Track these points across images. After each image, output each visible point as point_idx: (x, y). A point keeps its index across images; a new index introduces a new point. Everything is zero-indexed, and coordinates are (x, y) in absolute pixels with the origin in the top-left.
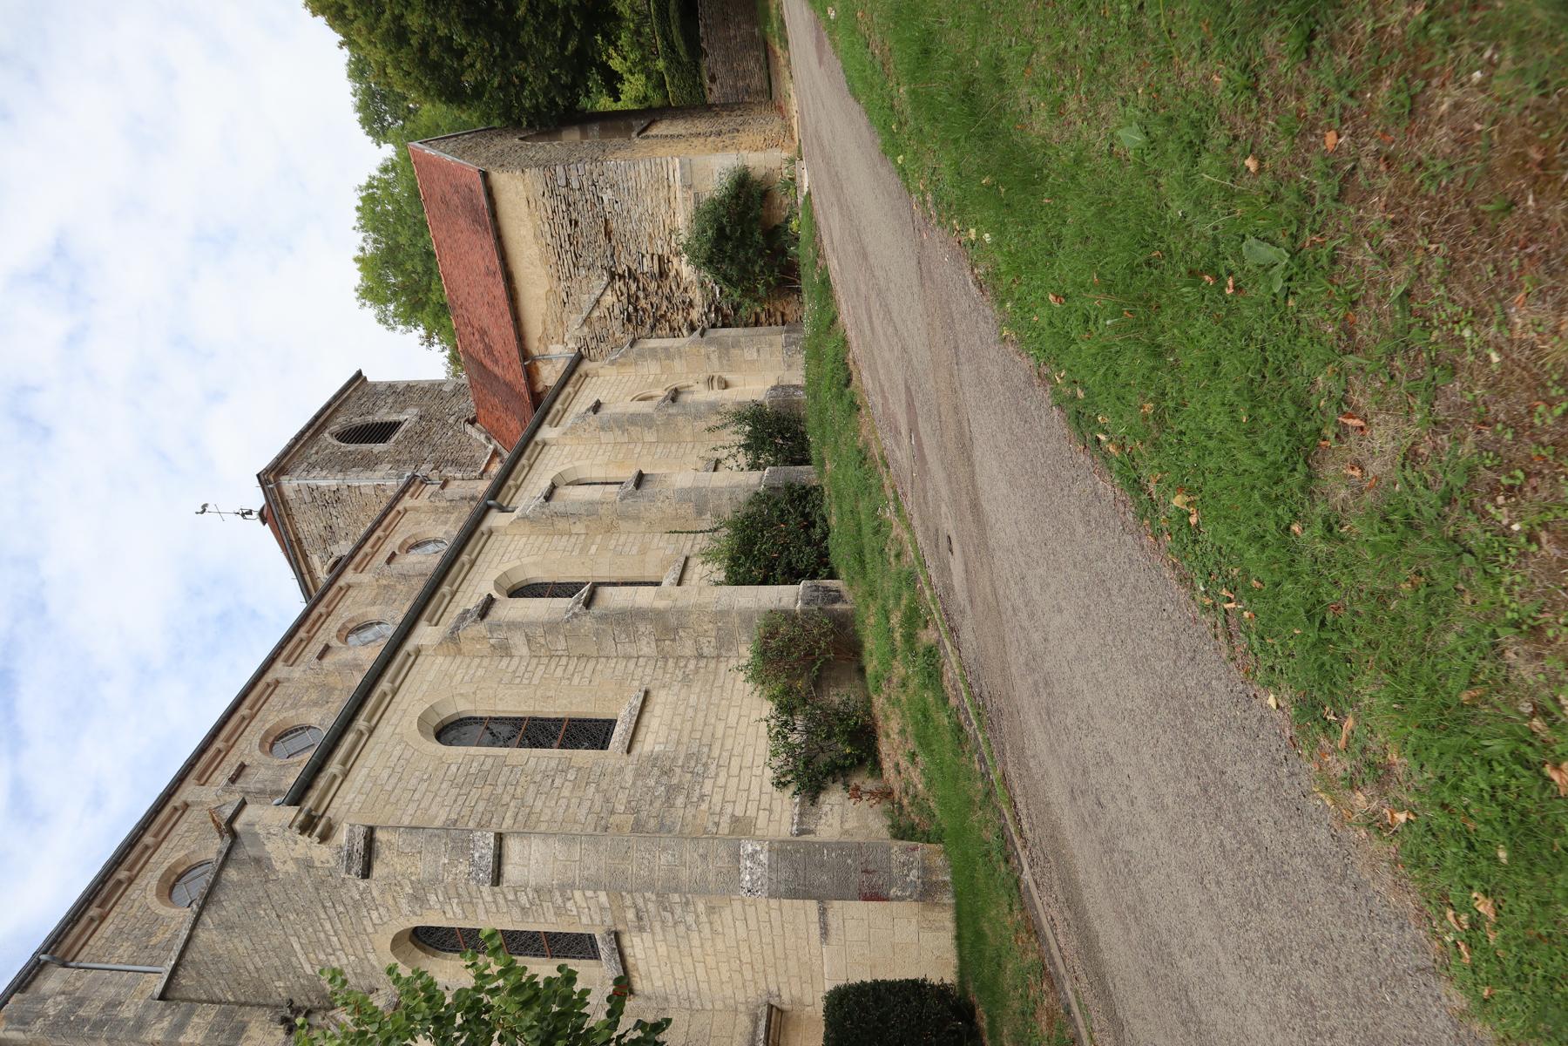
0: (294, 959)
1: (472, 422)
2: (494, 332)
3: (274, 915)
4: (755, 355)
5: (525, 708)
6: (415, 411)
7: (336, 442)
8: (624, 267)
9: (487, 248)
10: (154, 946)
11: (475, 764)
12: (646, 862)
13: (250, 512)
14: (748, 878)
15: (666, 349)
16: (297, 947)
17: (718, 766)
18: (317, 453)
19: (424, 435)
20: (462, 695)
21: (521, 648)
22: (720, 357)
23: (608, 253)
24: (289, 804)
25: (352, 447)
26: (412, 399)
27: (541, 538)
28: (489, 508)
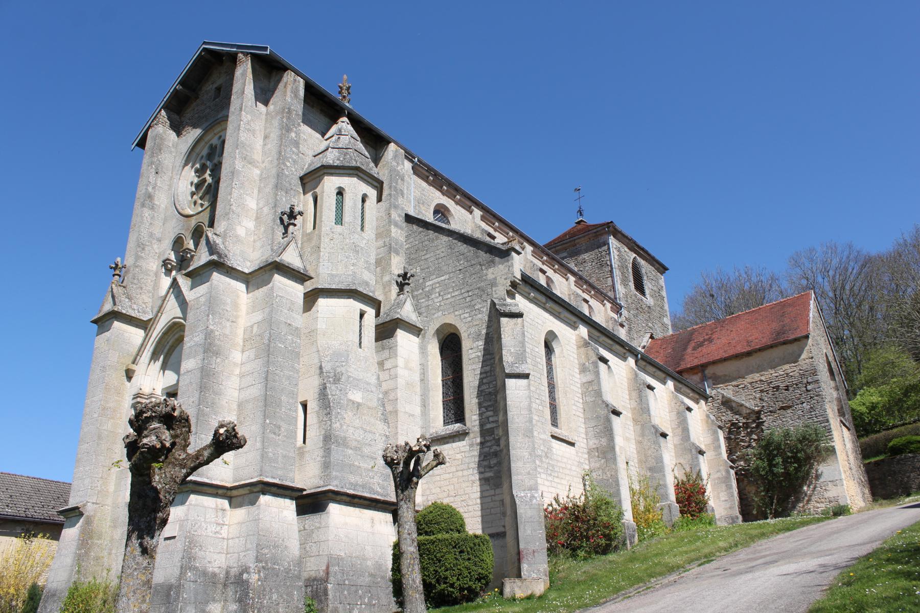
0: (435, 276)
1: (652, 337)
2: (713, 347)
3: (461, 268)
4: (723, 499)
5: (559, 382)
6: (652, 304)
7: (631, 261)
8: (765, 419)
9: (764, 340)
10: (419, 207)
11: (539, 360)
12: (523, 446)
13: (581, 215)
14: (523, 495)
15: (719, 446)
16: (443, 278)
17: (551, 481)
18: (625, 251)
19: (641, 310)
20: (563, 350)
21: (589, 377)
22: (719, 478)
23: (771, 409)
24: (522, 274)
25: (630, 270)
26: (658, 300)
27: (626, 384)
28: (637, 356)
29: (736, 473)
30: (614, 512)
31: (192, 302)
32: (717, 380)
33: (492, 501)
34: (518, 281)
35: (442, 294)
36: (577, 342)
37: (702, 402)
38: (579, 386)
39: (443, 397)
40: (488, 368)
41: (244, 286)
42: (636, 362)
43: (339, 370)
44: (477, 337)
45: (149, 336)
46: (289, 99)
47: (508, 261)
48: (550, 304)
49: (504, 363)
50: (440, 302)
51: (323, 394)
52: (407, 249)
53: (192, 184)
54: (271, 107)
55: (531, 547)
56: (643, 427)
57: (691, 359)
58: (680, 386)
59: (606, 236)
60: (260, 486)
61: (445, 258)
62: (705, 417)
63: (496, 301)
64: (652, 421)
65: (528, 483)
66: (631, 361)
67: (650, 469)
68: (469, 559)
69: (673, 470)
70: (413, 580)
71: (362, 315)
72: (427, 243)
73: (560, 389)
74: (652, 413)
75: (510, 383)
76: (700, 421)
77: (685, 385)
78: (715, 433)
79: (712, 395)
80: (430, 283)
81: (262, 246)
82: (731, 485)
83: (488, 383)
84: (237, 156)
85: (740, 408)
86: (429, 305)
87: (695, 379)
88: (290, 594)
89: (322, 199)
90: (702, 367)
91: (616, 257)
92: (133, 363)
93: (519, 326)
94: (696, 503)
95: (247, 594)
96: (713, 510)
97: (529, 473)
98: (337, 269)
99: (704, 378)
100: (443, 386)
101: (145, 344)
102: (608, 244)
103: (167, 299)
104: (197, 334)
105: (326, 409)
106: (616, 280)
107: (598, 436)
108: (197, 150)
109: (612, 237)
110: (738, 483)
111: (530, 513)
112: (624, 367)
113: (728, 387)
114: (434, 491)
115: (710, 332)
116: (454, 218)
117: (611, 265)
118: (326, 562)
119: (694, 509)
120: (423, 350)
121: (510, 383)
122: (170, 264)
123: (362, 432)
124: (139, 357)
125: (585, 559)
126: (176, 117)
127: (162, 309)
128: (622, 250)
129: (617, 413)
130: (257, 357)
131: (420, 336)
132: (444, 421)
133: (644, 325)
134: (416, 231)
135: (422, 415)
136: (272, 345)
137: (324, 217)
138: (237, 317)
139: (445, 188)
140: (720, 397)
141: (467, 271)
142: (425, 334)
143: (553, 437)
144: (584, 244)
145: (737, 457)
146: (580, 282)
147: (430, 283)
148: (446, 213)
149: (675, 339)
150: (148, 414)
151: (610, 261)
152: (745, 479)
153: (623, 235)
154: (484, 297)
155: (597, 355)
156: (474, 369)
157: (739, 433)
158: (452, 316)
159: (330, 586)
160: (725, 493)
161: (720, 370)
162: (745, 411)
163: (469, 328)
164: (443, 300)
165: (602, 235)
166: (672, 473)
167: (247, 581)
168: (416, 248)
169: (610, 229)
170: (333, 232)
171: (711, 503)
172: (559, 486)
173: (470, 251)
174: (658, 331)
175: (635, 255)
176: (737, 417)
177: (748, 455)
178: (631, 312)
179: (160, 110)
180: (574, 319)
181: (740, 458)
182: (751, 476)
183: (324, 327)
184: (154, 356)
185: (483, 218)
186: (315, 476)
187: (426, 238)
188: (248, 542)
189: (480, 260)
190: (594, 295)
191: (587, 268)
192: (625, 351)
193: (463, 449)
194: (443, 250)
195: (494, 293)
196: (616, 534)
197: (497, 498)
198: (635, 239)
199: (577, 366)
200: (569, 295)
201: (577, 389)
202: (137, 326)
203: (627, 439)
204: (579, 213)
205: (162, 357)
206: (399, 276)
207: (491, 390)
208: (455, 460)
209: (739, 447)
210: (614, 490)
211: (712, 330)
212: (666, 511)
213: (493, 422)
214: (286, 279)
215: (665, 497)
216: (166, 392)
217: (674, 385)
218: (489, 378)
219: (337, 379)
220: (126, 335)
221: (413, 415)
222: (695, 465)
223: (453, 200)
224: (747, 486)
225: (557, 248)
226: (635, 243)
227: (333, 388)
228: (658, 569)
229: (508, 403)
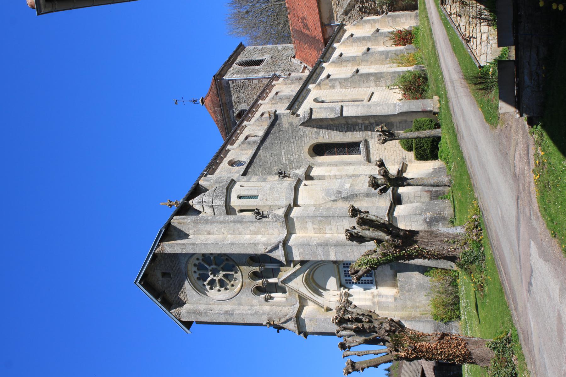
0: (281, 158)
1: (294, 57)
3: (279, 143)
4: (405, 20)
6: (269, 55)
7: (240, 67)
15: (373, 20)
16: (283, 153)
20: (323, 96)
21: (337, 84)
22: (392, 22)
24: (287, 110)
25: (246, 68)
28: (321, 62)
29: (390, 11)
30: (408, 74)
31: (301, 257)
32: (331, 18)
33: (399, 127)
34: (291, 111)
35: (291, 154)
36: (318, 90)
37: (345, 27)
38: (342, 90)
39: (346, 155)
40: (335, 128)
41: (293, 235)
42: (324, 62)
43: (335, 192)
44: (318, 133)
45: (310, 298)
46: (189, 221)
47: (280, 116)
48: (300, 99)
49: (335, 117)
50: (296, 155)
51: (346, 199)
52: (262, 175)
53: (219, 291)
54: (191, 232)
55: (421, 106)
56: (363, 61)
57: (317, 32)
58: (336, 40)
59: (223, 81)
60: (390, 215)
61: (272, 152)
62: (355, 27)
63: (301, 123)
64: (360, 55)
65: (392, 107)
66: (324, 65)
67: (386, 58)
68: (423, 125)
69: (387, 47)
70: (428, 133)
71: (305, 185)
72: (261, 163)
73: (344, 98)
74: (355, 55)
75: (345, 114)
76: (357, 30)
77: (335, 37)
78: (365, 21)
79: (341, 21)
80: (284, 160)
81: (272, 228)
82: (397, 15)
83: (342, 128)
84: (223, 243)
85: (351, 5)
86: (297, 161)
87: (329, 31)
88: (436, 204)
89: (242, 206)
90: (323, 25)
91: (239, 76)
92: (323, 308)
93: (317, 110)
94: (406, 36)
95: (435, 218)
96: (411, 27)
97: (388, 107)
98: (283, 196)
99: (329, 25)
100: (340, 155)
101: (313, 301)
102: (229, 80)
103: (291, 287)
104: (318, 252)
105: (354, 197)
106: (255, 77)
107: (369, 82)
108: (199, 288)
109: (224, 77)
110: (396, 11)
111: (406, 106)
112: (328, 69)
113: (337, 11)
114: (393, 159)
115: (297, 18)
116: (235, 158)
117: (244, 79)
118: (423, 192)
119: (409, 37)
120: (320, 165)
121: (345, 114)
122: (267, 296)
123: (365, 184)
124: (320, 305)
125: (428, 87)
126: (173, 306)
127: (296, 290)
128: (232, 72)
129: (357, 71)
130: (330, 224)
131: (313, 166)
132: (358, 154)
133: (285, 62)
134: (253, 170)
135: (354, 165)
136: (325, 215)
137: (254, 204)
138: (309, 236)
139: (218, 161)
140: (343, 16)
141: (282, 139)
142: (312, 164)
143: (369, 100)
144: (226, 97)
145: (380, 10)
146: (262, 97)
147: (284, 160)
148: (232, 162)
149: (298, 42)
150: (373, 181)
151: (241, 80)
152: (394, 6)
153: (222, 70)
154: (297, 129)
155: (326, 79)
156: (334, 136)
157: (366, 7)
158: (304, 148)
159: (434, 190)
160: (401, 19)
161: (325, 15)
162: (353, 2)
163: (312, 139)
164: (295, 153)
165: (221, 84)
166: (389, 47)
167: (430, 218)
168: (263, 169)
169: (218, 77)
170: (263, 199)
171: (407, 27)
172: (394, 99)
173: (271, 137)
174: (288, 53)
175: (234, 64)
176: (356, 7)
177: (380, 3)
178: (277, 69)
179: (171, 313)
180: (305, 90)
181: (381, 8)
182: (393, 3)
183: (313, 201)
184: (320, 295)
185: (232, 144)
186: (385, 202)
187: (258, 163)
188: (413, 220)
189: (277, 131)
190: (269, 90)
191: (244, 96)
192: (319, 68)
193: (373, 143)
194: (267, 153)
195: (296, 124)
196: (418, 74)
197: (398, 125)
198: (224, 62)
199: (331, 90)
200: (272, 104)
201: (343, 91)
202: (303, 309)
203: (369, 68)
204: (195, 102)
205: (320, 290)
206: (279, 177)
207: (345, 127)
208: (378, 147)
209: (374, 8)
210: (396, 75)
211: (295, 17)
212: (409, 51)
213: (361, 126)
214: (292, 213)
215: (402, 51)
216: (339, 288)
217: (336, 43)
218: (340, 128)
219: (340, 192)
220: (307, 313)
221: (355, 169)
222: (385, 35)
223: (224, 158)
224: (398, 6)
225: (226, 117)
226: (226, 63)
227: (344, 194)
228: (433, 52)
229: (354, 115)
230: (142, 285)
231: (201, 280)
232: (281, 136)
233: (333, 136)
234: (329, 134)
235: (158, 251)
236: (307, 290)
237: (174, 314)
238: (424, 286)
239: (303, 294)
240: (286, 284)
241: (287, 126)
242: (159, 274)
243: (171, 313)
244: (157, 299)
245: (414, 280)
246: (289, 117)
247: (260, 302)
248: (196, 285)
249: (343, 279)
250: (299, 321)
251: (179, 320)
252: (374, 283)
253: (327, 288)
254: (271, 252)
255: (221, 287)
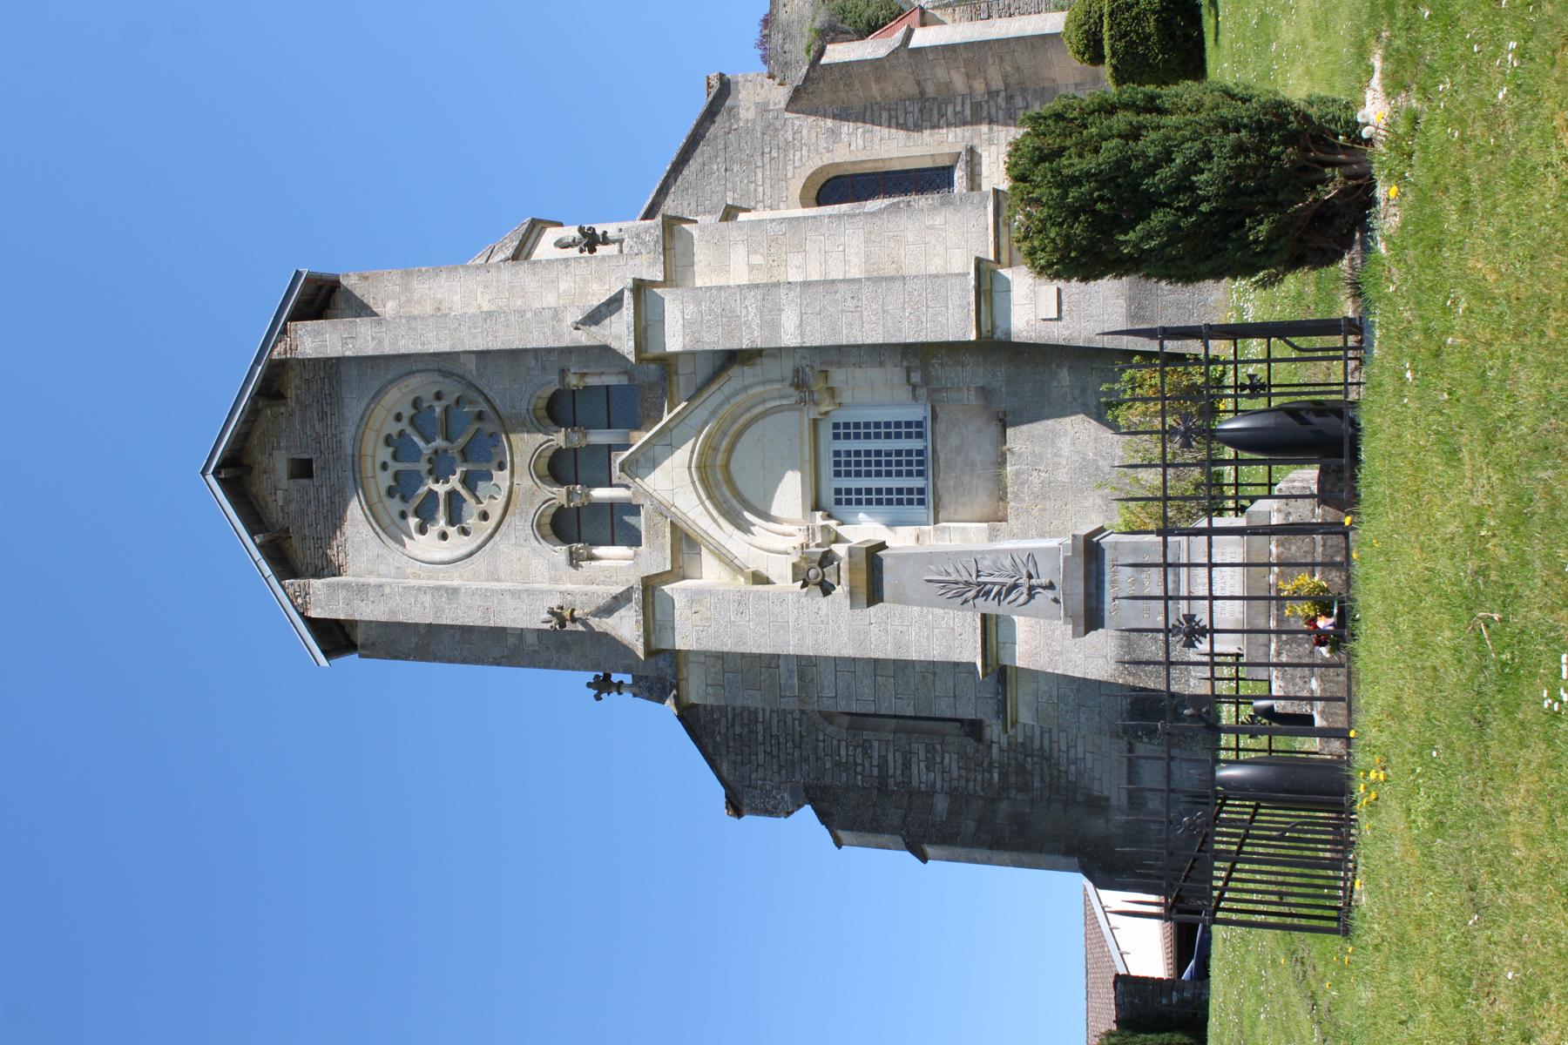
3: (723, 168)
44: (834, 134)
108: (386, 521)
154: (778, 124)
156: (881, 140)
158: (792, 182)
164: (763, 202)
173: (702, 152)
184: (744, 527)
194: (685, 203)
195: (777, 107)
205: (746, 514)
207: (916, 110)
230: (222, 482)
231: (393, 484)
232: (731, 148)
233: (877, 140)
234: (867, 135)
235: (279, 354)
236: (702, 503)
237: (291, 591)
238: (1097, 468)
239: (684, 518)
240: (637, 480)
241: (751, 115)
242: (280, 464)
243: (283, 587)
244: (252, 535)
245: (1065, 445)
246: (759, 87)
247: (555, 567)
248: (379, 508)
249: (830, 484)
250: (653, 603)
251: (302, 615)
252: (929, 498)
253: (774, 512)
254: (597, 323)
255: (451, 522)
